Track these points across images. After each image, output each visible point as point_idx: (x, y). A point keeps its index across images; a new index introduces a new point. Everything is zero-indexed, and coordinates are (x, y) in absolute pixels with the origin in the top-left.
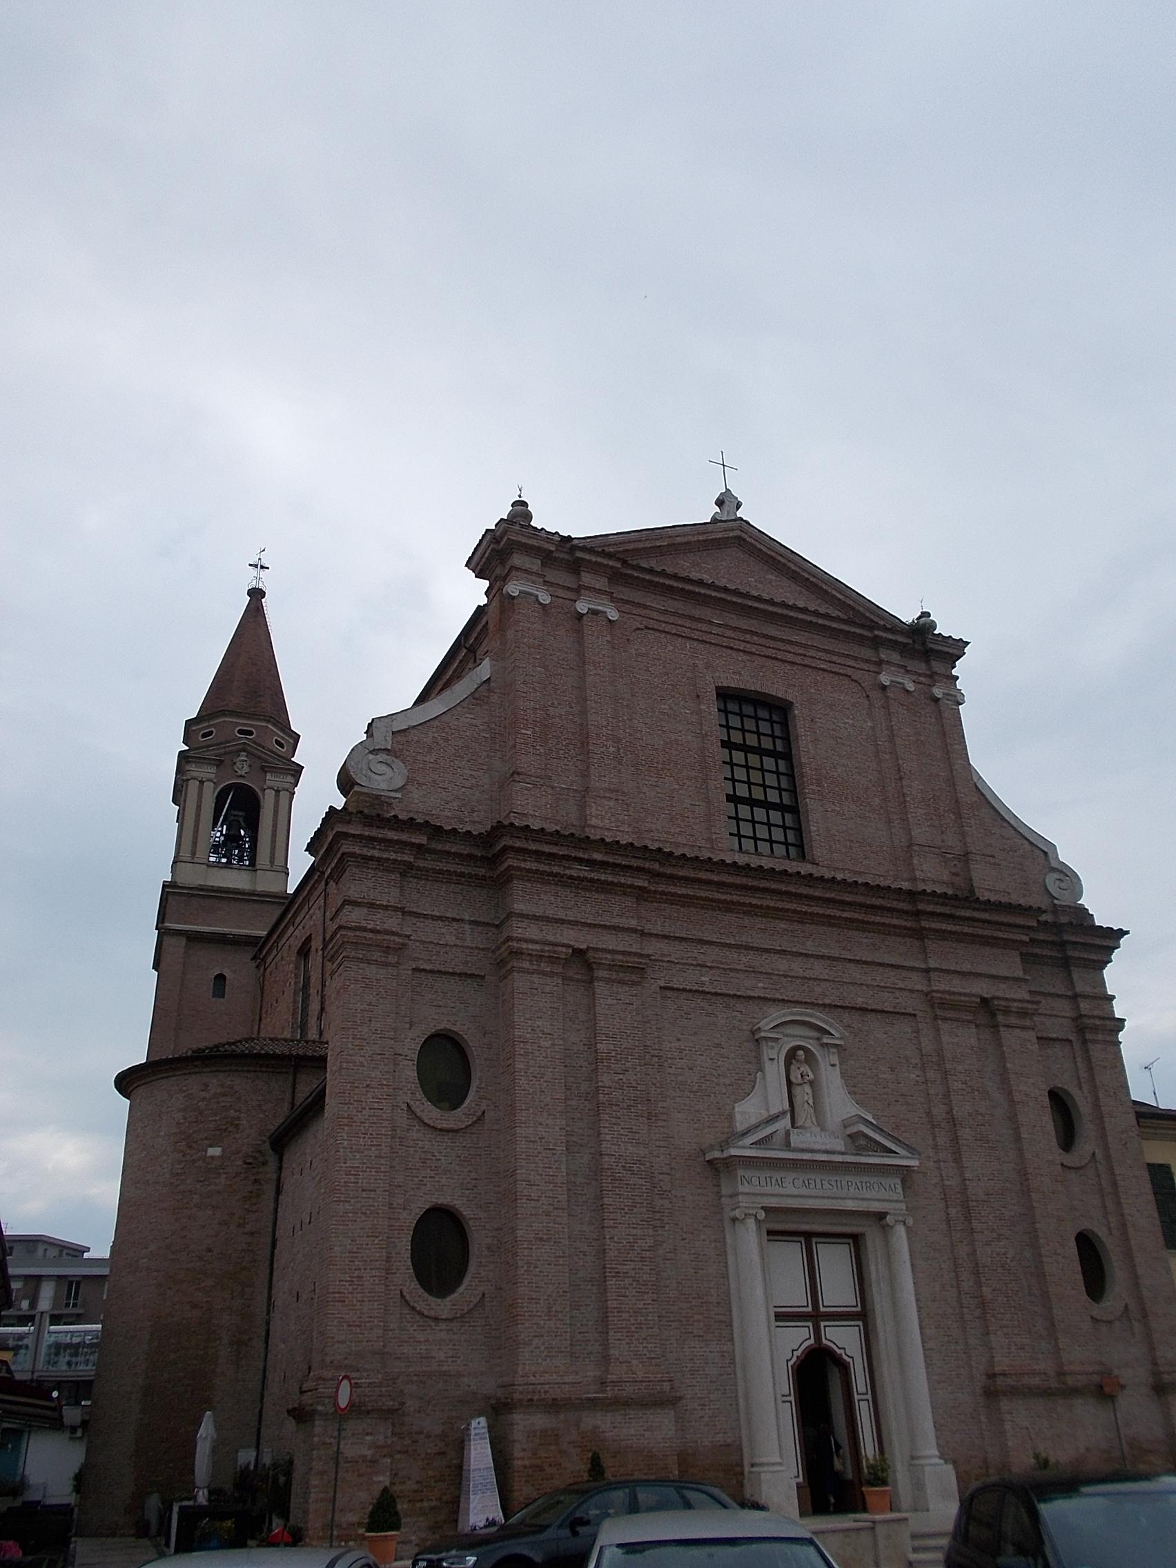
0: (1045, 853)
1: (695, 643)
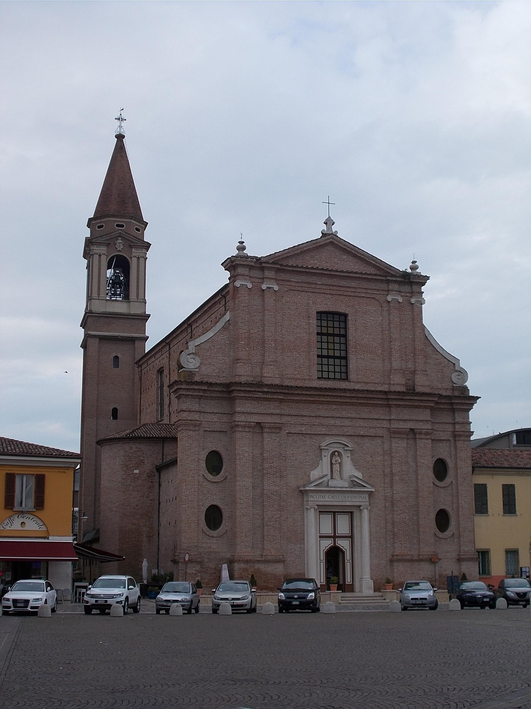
0: (454, 364)
1: (309, 293)
